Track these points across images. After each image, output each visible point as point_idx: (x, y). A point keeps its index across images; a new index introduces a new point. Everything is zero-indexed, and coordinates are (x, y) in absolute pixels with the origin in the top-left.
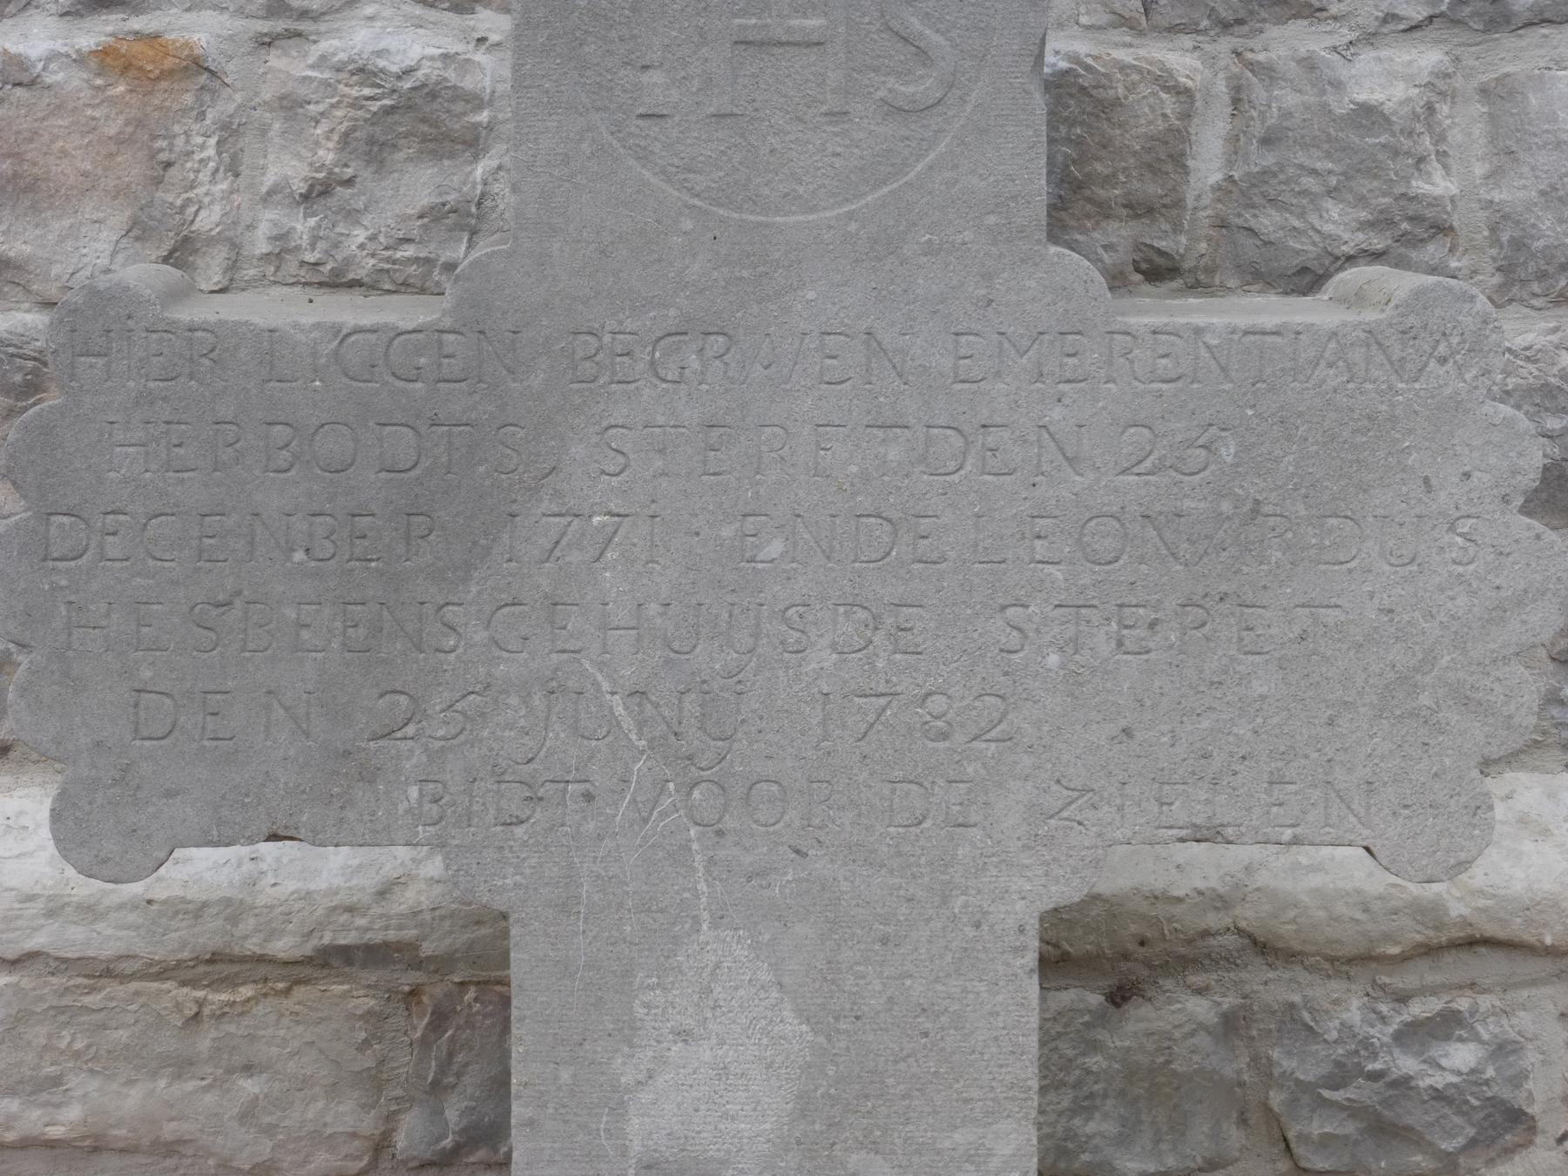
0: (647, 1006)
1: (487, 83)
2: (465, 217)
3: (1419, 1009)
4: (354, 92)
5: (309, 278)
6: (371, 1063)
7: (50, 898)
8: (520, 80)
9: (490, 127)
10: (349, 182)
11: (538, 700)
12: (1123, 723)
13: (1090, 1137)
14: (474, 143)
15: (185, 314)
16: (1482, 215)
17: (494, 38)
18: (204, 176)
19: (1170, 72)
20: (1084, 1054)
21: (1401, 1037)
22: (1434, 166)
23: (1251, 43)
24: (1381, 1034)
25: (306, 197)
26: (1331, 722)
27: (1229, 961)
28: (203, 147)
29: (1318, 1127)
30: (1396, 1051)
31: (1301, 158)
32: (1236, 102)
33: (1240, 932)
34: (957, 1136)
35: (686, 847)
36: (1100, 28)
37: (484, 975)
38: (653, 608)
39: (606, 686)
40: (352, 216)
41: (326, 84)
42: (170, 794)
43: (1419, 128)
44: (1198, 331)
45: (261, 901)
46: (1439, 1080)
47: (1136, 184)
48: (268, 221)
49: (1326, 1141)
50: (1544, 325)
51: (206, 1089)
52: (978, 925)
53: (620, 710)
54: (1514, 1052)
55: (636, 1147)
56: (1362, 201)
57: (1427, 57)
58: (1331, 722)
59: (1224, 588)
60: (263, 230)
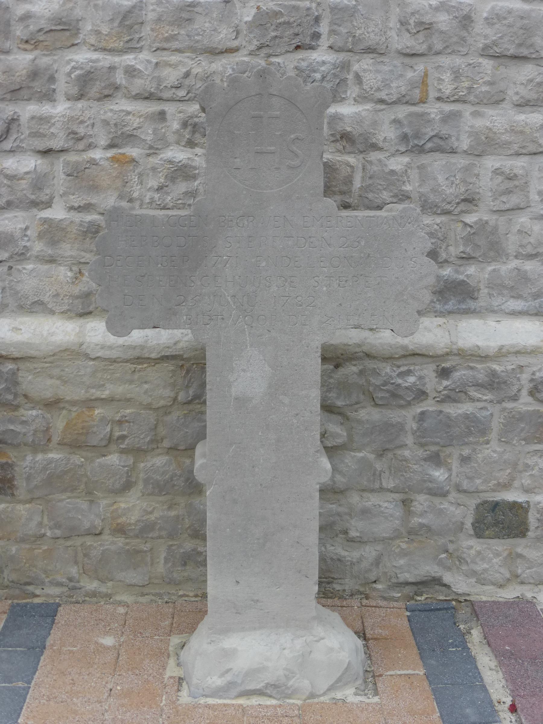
0: (236, 364)
1: (198, 164)
2: (193, 194)
3: (403, 369)
4: (168, 166)
5: (158, 207)
6: (172, 381)
7: (102, 345)
8: (207, 161)
9: (198, 174)
10: (167, 186)
11: (212, 298)
12: (340, 303)
13: (330, 397)
14: (194, 177)
15: (134, 212)
16: (417, 195)
17: (199, 154)
18: (135, 185)
19: (349, 162)
20: (329, 379)
21: (398, 375)
22: (407, 183)
23: (367, 156)
24: (394, 374)
25: (157, 190)
26: (384, 302)
27: (360, 359)
28: (134, 178)
29: (380, 395)
30: (397, 379)
31: (378, 181)
32: (363, 169)
33: (363, 352)
34: (303, 392)
35: (244, 330)
36: (334, 152)
37: (198, 362)
38: (237, 277)
39: (227, 295)
40: (168, 194)
41: (162, 164)
42: (132, 318)
43: (404, 175)
44: (356, 216)
45: (148, 346)
46: (407, 385)
47: (342, 187)
48: (149, 195)
49: (382, 398)
50: (431, 219)
51: (137, 387)
52: (308, 347)
53: (230, 300)
54: (423, 378)
55: (234, 394)
56: (391, 191)
57: (405, 159)
58: (384, 302)
59: (362, 273)
60: (148, 197)
